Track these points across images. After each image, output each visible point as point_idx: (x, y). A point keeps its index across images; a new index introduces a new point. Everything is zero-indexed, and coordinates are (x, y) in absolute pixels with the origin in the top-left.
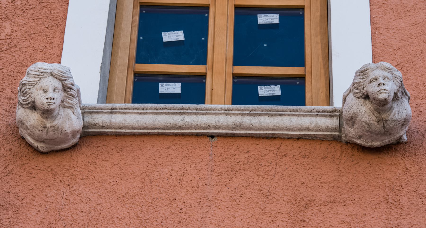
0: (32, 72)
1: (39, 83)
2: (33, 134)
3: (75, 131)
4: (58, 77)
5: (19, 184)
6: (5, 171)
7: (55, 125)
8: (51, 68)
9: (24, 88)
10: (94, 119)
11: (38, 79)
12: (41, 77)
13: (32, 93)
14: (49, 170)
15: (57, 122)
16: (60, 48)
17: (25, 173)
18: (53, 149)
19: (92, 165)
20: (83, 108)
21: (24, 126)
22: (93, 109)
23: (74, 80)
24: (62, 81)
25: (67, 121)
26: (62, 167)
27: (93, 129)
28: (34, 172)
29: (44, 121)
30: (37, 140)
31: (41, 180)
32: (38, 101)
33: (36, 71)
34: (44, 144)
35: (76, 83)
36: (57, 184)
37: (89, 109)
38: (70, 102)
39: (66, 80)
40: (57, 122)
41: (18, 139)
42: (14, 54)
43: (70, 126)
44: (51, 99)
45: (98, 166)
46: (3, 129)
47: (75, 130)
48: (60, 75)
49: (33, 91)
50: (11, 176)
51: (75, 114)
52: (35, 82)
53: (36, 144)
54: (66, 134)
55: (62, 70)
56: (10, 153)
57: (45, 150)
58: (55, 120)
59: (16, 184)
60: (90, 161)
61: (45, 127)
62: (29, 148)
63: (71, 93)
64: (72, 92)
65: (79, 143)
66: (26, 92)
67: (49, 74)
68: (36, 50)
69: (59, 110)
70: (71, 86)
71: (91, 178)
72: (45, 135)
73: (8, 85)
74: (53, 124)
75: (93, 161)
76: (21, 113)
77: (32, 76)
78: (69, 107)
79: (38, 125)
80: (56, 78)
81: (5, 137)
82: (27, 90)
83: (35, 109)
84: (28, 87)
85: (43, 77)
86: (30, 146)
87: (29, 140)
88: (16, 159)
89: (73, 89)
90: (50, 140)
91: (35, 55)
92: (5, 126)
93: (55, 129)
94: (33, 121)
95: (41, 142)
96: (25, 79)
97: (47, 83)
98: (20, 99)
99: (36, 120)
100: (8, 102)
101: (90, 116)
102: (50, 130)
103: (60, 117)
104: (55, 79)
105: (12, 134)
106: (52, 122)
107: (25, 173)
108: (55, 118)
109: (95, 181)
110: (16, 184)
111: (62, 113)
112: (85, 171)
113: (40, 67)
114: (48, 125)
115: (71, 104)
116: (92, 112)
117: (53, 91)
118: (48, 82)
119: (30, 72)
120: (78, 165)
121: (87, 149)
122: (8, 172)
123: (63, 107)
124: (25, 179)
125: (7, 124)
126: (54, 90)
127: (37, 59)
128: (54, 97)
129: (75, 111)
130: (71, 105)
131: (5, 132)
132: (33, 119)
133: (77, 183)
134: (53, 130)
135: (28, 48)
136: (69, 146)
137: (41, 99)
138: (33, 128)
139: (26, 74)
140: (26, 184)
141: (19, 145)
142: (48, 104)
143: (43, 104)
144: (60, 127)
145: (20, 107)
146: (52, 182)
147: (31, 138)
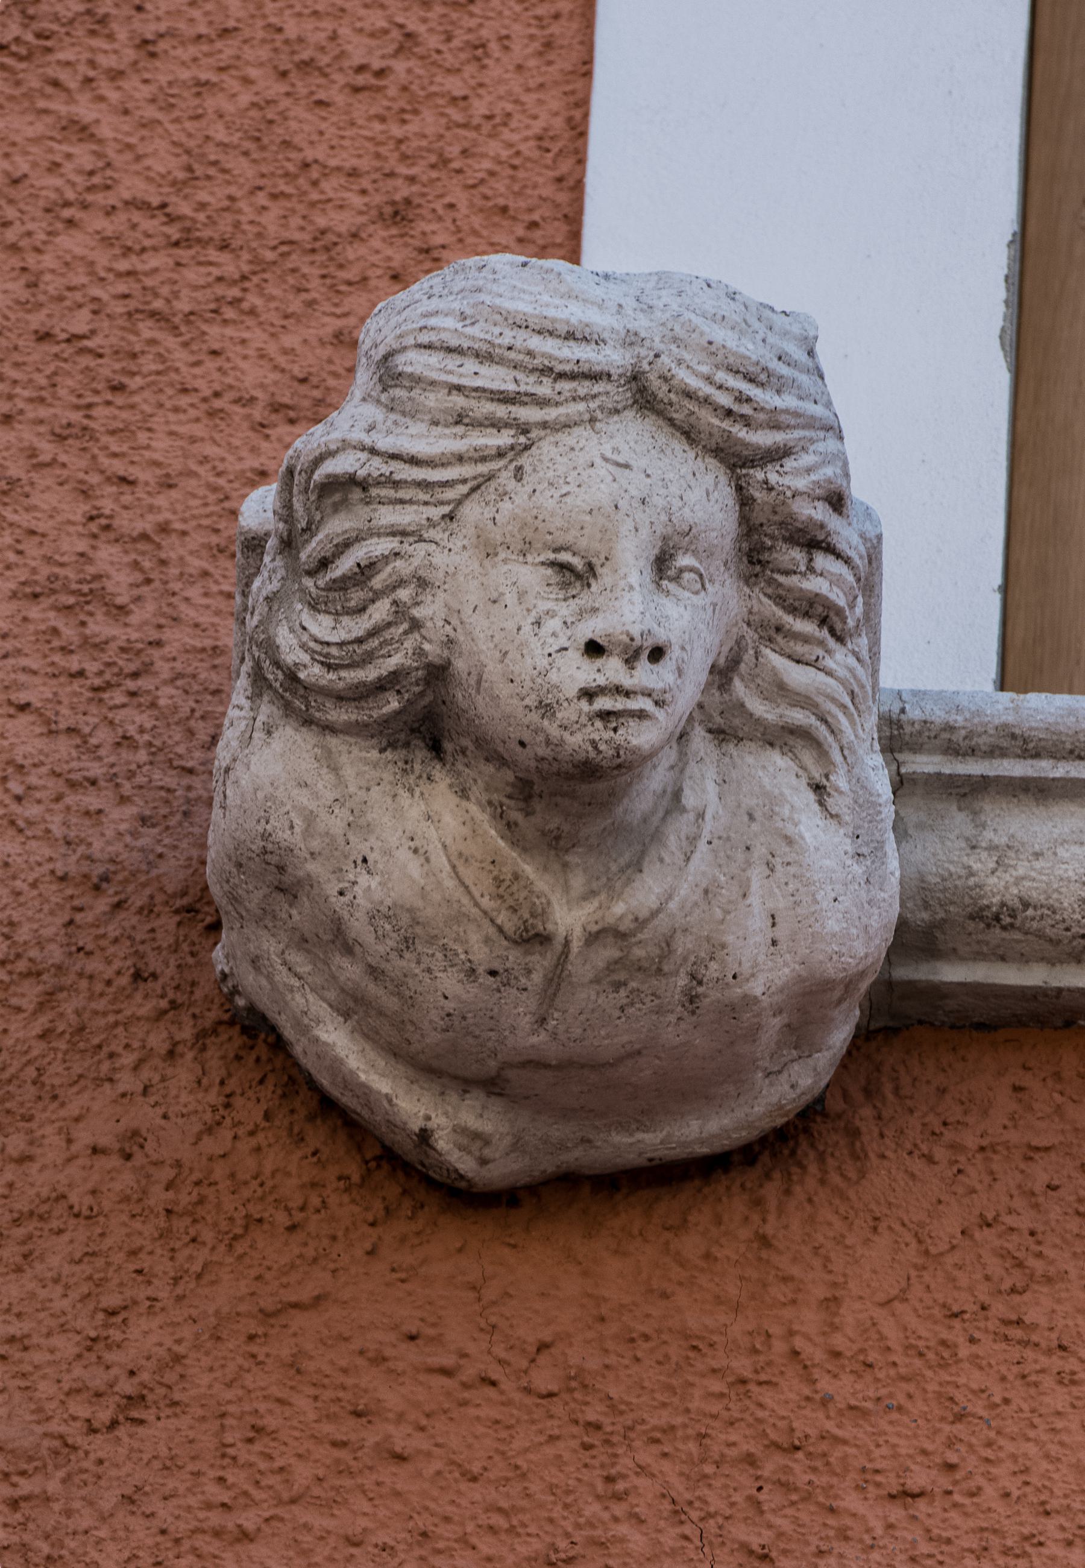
0: (434, 359)
1: (506, 478)
2: (391, 1003)
3: (827, 985)
4: (709, 419)
5: (249, 1520)
6: (98, 1379)
7: (641, 923)
8: (642, 324)
9: (337, 526)
10: (1002, 856)
11: (504, 439)
12: (528, 414)
13: (423, 583)
14: (544, 1379)
15: (656, 890)
16: (563, 62)
17: (301, 1402)
18: (575, 1157)
19: (988, 1347)
20: (896, 737)
21: (298, 915)
22: (995, 752)
23: (851, 446)
24: (737, 461)
25: (756, 875)
26: (675, 1351)
27: (979, 956)
28: (392, 1398)
29: (528, 869)
30: (430, 1070)
31: (475, 1492)
32: (493, 671)
33: (485, 357)
34: (496, 1105)
35: (858, 491)
36: (637, 1540)
37: (953, 750)
38: (798, 676)
39: (778, 455)
40: (656, 890)
41: (201, 1035)
42: (85, 110)
43: (781, 933)
44: (630, 661)
45: (1056, 1362)
46: (39, 924)
47: (831, 971)
48: (724, 400)
49: (440, 559)
50: (158, 1433)
51: (838, 803)
52: (467, 471)
53: (413, 1107)
54: (731, 1010)
55: (750, 349)
56: (126, 1180)
57: (502, 1169)
58: (637, 866)
59: (215, 1518)
60: (963, 1301)
61: (534, 938)
62: (317, 1136)
63: (815, 585)
64: (827, 580)
65: (835, 1104)
66: (366, 570)
67: (614, 393)
68: (306, 66)
69: (680, 767)
70: (820, 512)
71: (990, 1491)
72: (525, 1022)
73: (47, 449)
74: (619, 908)
75: (999, 1308)
76: (272, 774)
77: (432, 400)
78: (784, 738)
79: (460, 917)
80: (689, 434)
81: (69, 1006)
82: (381, 546)
83: (436, 748)
84: (387, 516)
85: (551, 414)
86: (330, 1112)
87: (336, 1065)
88: (202, 1255)
89: (831, 550)
90: (565, 1066)
91: (302, 122)
92: (50, 888)
93: (632, 956)
94: (414, 867)
95: (466, 1084)
96: (354, 427)
97: (600, 488)
98: (284, 638)
99: (440, 861)
100: (69, 633)
101: (959, 821)
102: (584, 966)
103: (693, 840)
104: (678, 445)
105: (138, 976)
106: (610, 886)
107: (301, 1402)
108: (639, 846)
109: (1030, 1523)
110: (215, 1518)
111: (712, 789)
112: (918, 1407)
113: (522, 306)
114: (569, 918)
115: (804, 701)
116: (982, 786)
117: (648, 575)
118: (603, 470)
119: (414, 362)
120: (839, 1341)
121: (917, 1165)
122: (127, 1387)
123: (720, 735)
124: (303, 1473)
125: (69, 864)
126: (662, 565)
127: (327, 172)
128: (661, 635)
129: (840, 780)
130: (799, 717)
131: (55, 954)
132: (410, 844)
133: (844, 1536)
134: (612, 966)
135: (228, 49)
136: (742, 1136)
137: (522, 648)
138: (408, 942)
139: (364, 378)
140: (319, 1521)
141: (214, 1097)
142: (604, 703)
143: (546, 709)
144: (683, 945)
145: (267, 710)
146: (593, 1509)
147: (369, 1035)
